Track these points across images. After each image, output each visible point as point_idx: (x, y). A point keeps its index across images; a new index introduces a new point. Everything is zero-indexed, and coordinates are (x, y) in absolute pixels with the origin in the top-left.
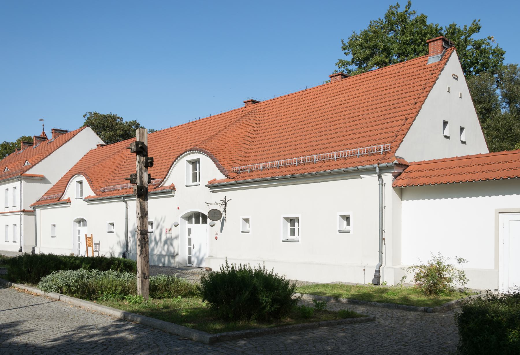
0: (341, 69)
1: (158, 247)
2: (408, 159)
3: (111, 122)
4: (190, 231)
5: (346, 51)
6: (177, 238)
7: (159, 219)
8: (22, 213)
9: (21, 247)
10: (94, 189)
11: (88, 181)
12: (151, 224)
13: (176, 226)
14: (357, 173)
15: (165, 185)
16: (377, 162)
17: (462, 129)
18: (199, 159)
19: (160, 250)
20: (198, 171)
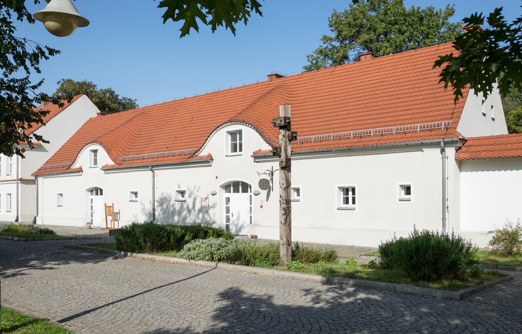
0: (326, 45)
1: (191, 216)
2: (466, 136)
3: (86, 90)
4: (228, 200)
5: (333, 28)
6: (213, 207)
7: (192, 188)
8: (19, 182)
9: (18, 217)
10: (113, 157)
11: (105, 149)
12: (298, 190)
13: (213, 195)
14: (419, 147)
15: (200, 155)
16: (441, 136)
17: (492, 107)
18: (241, 130)
19: (194, 218)
20: (238, 142)
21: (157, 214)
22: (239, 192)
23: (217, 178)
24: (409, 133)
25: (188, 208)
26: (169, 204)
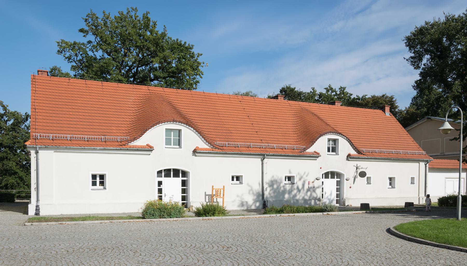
1: (301, 194)
4: (160, 183)
19: (303, 195)
21: (266, 193)
22: (170, 177)
23: (321, 168)
24: (73, 140)
25: (298, 188)
26: (280, 185)
